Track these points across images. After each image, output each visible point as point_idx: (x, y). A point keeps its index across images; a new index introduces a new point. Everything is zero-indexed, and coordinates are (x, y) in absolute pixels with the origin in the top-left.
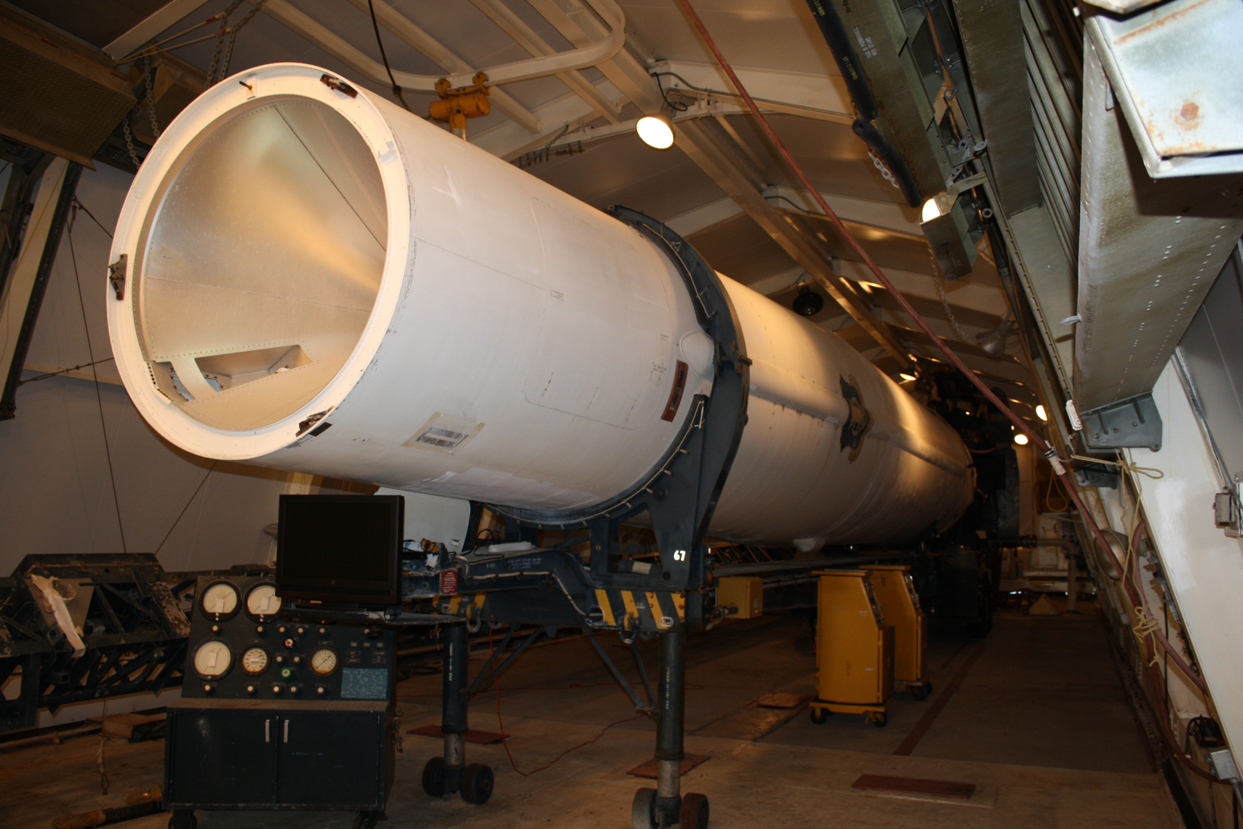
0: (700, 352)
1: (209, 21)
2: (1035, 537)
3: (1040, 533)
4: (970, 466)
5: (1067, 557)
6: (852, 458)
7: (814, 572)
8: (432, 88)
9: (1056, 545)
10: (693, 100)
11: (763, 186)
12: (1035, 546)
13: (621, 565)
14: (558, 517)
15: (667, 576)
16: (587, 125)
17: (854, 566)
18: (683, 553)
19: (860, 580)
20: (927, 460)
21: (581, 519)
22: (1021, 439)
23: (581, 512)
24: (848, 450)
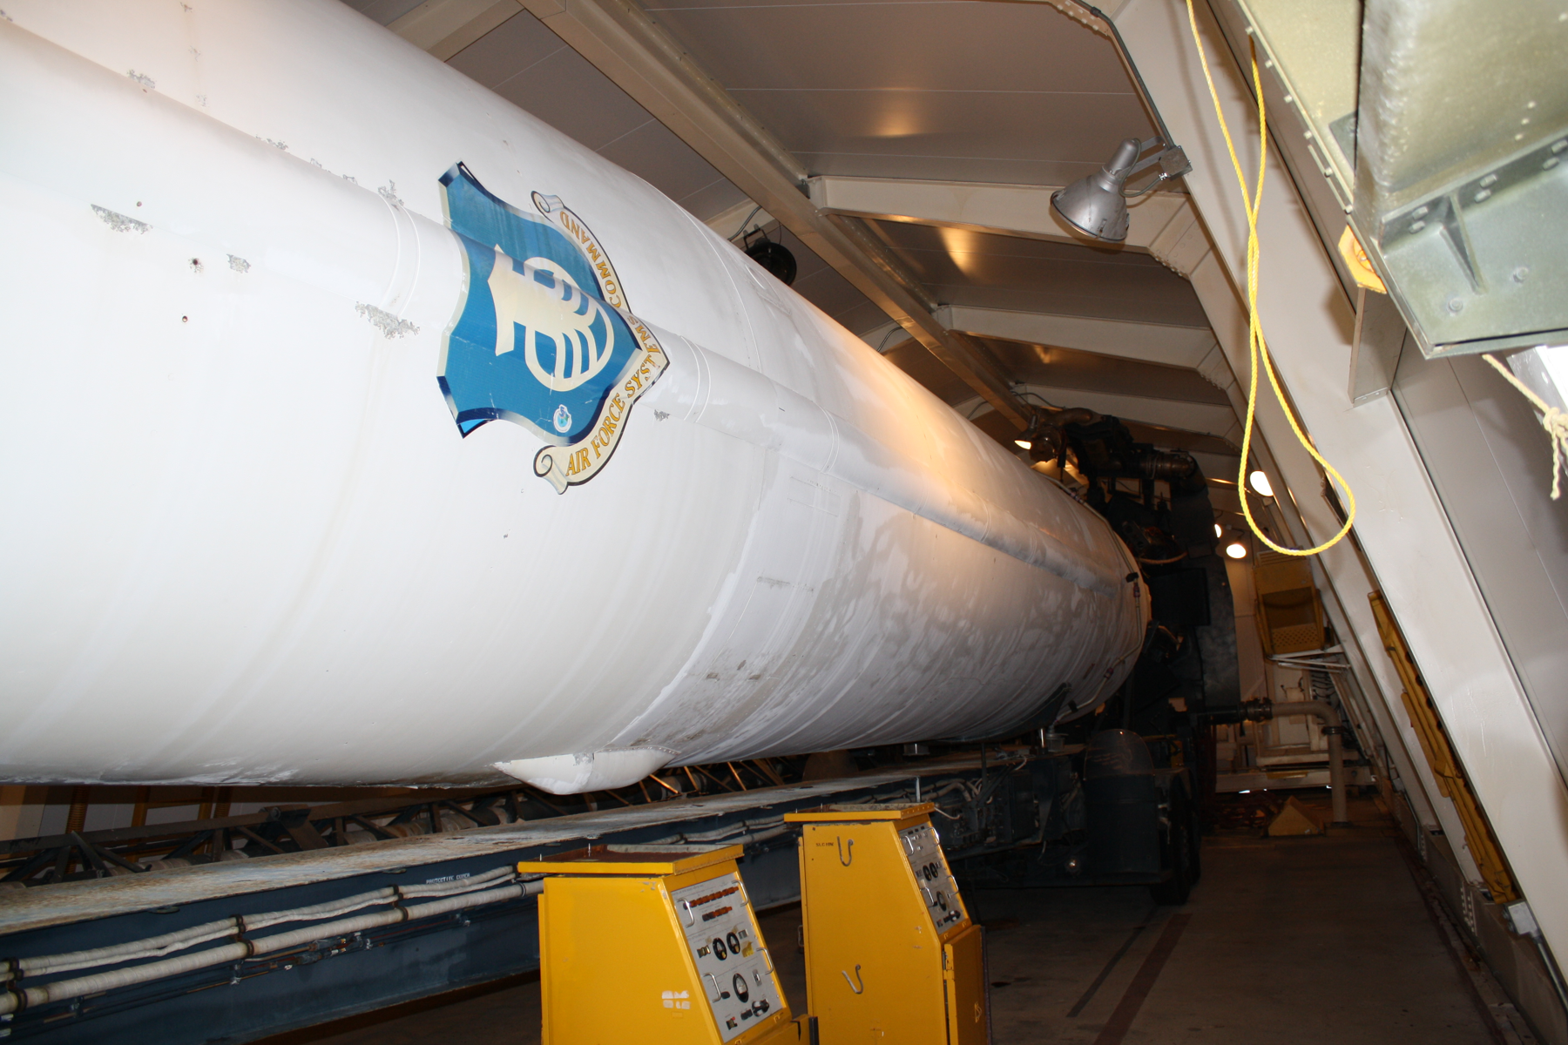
2: (1267, 702)
3: (1279, 695)
5: (1325, 731)
12: (1269, 717)
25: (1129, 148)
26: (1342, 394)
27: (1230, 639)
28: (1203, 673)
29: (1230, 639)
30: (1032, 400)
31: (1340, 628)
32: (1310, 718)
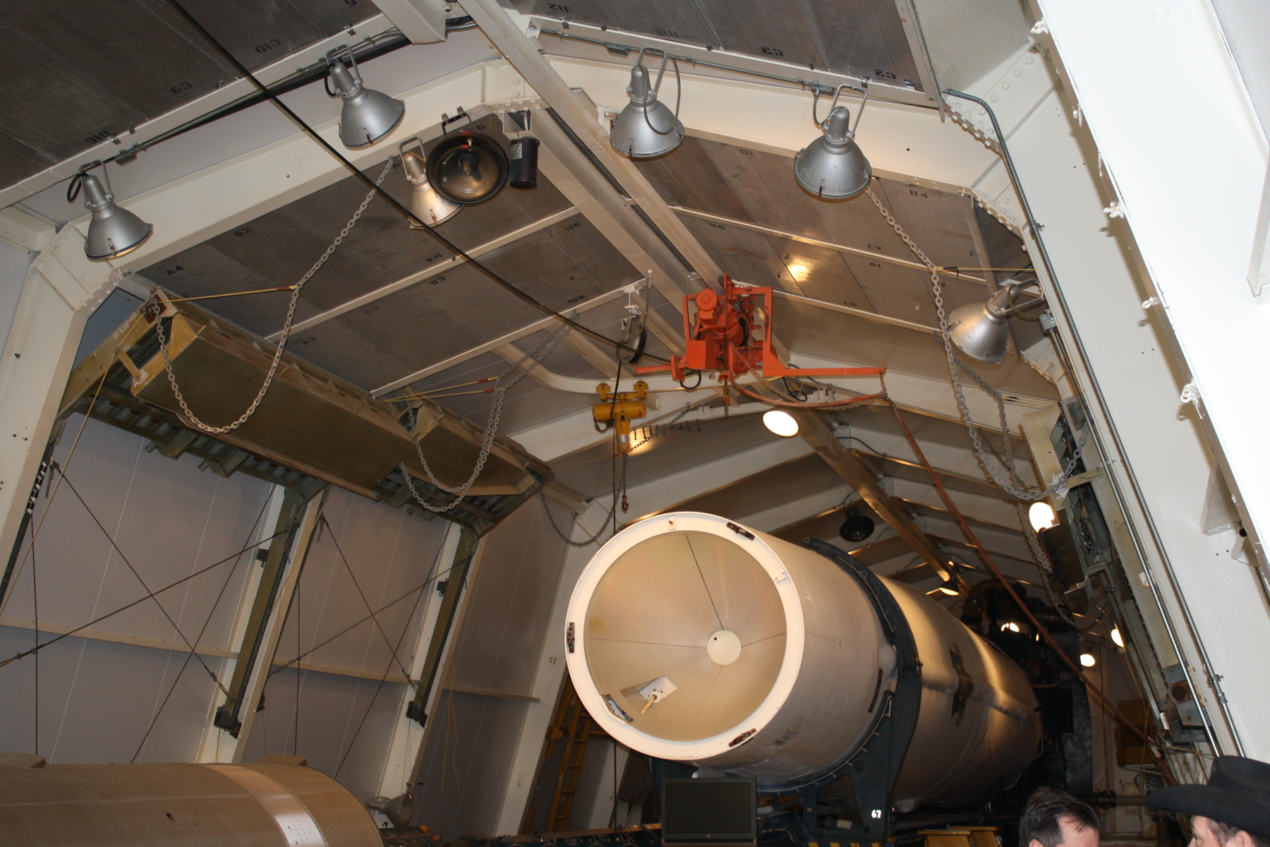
0: (888, 656)
1: (481, 382)
2: (1113, 794)
3: (1117, 789)
4: (1036, 710)
5: (1155, 819)
6: (958, 724)
7: (920, 832)
8: (593, 391)
9: (1139, 804)
10: (811, 389)
11: (835, 425)
12: (1113, 805)
13: (827, 823)
14: (775, 786)
15: (867, 830)
16: (706, 405)
17: (963, 824)
18: (879, 812)
19: (964, 838)
20: (1006, 712)
21: (796, 788)
22: (1087, 660)
23: (796, 782)
24: (956, 715)
25: (1166, 727)
26: (1196, 526)
27: (1087, 744)
28: (1065, 769)
29: (1087, 744)
30: (855, 445)
31: (1197, 680)
32: (1143, 809)
